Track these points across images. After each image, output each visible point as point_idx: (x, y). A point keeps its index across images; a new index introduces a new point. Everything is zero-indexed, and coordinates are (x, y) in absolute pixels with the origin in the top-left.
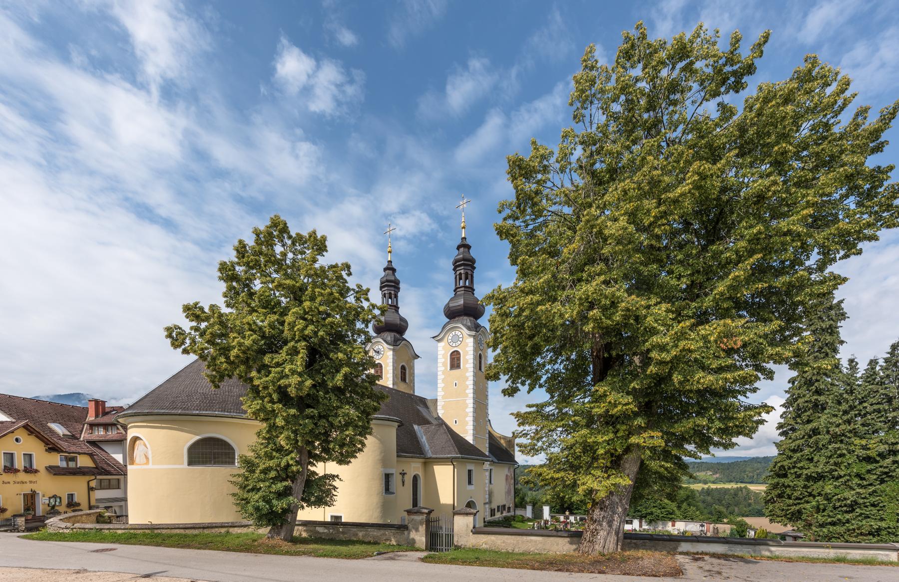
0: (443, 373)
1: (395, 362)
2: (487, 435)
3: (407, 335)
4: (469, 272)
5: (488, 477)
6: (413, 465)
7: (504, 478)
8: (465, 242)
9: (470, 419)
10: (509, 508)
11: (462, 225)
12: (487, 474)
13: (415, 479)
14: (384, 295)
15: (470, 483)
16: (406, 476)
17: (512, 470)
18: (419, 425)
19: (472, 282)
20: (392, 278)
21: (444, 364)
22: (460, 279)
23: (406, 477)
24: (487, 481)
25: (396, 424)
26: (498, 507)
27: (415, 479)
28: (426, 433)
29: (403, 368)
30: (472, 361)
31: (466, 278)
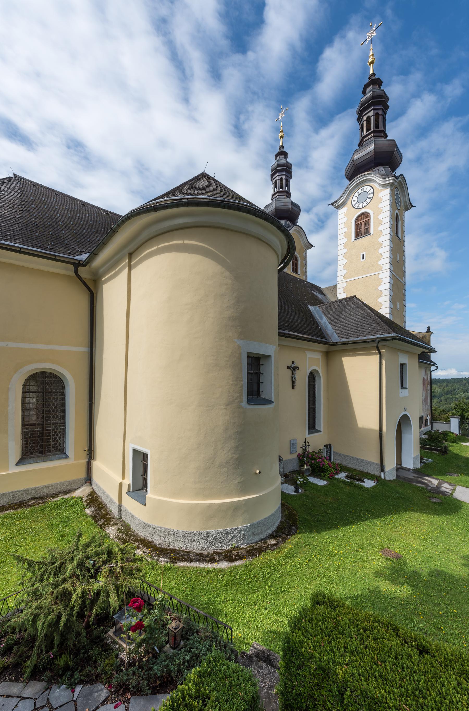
0: (345, 245)
4: (381, 112)
6: (310, 355)
10: (426, 420)
11: (370, 60)
13: (312, 377)
16: (297, 372)
17: (428, 373)
20: (284, 161)
21: (347, 235)
23: (298, 374)
27: (312, 377)
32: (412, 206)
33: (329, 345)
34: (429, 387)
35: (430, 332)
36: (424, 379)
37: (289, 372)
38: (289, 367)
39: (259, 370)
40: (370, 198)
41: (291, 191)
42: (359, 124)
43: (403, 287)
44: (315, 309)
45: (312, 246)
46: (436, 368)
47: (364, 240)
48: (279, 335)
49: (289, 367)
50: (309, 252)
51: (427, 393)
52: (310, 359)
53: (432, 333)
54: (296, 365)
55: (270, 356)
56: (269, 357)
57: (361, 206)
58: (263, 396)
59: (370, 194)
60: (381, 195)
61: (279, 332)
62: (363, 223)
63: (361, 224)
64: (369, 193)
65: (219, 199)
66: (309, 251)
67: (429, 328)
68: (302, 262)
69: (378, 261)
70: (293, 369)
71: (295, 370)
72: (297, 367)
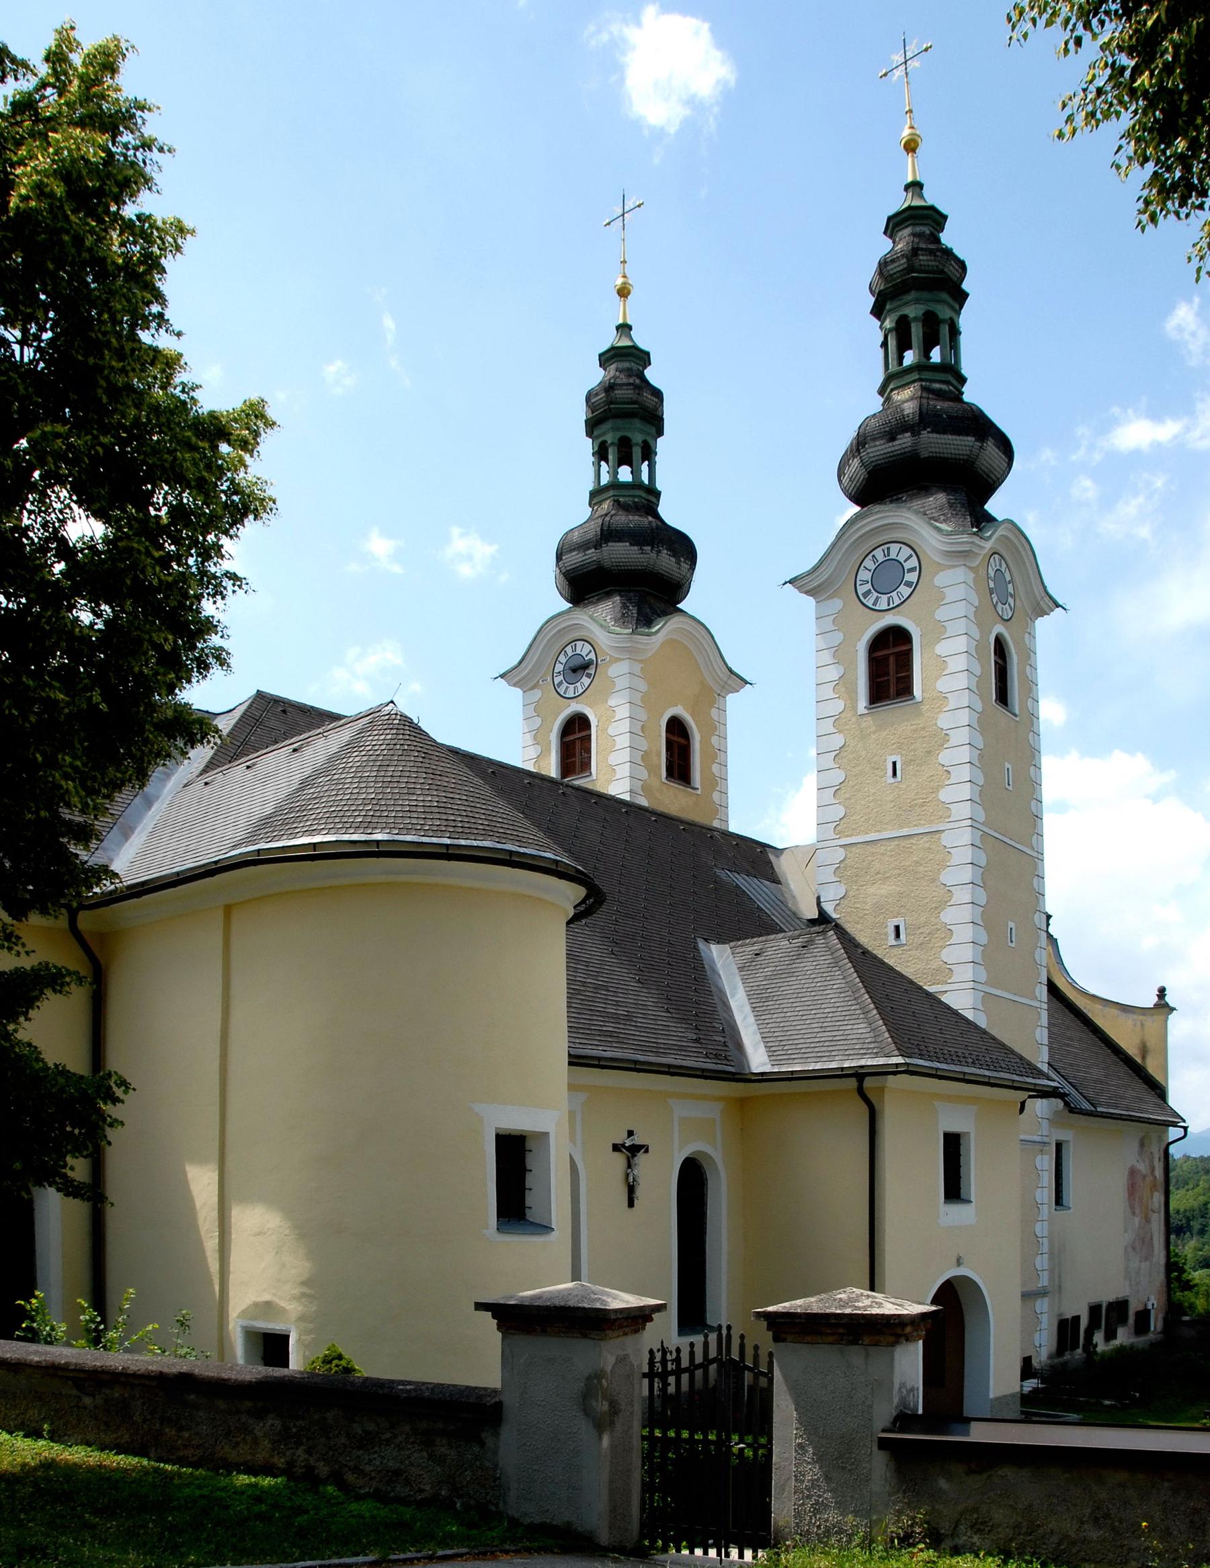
5: (1048, 1179)
9: (960, 916)
12: (1046, 1162)
13: (693, 1179)
14: (601, 454)
15: (954, 1191)
16: (641, 1158)
18: (720, 941)
24: (1046, 1194)
25: (571, 893)
26: (1095, 1310)
34: (1158, 1197)
35: (1167, 1005)
36: (1133, 1172)
37: (620, 1160)
38: (616, 1148)
40: (908, 584)
43: (1035, 867)
46: (1181, 1132)
48: (570, 1064)
49: (616, 1148)
51: (1148, 1220)
53: (1173, 1009)
54: (637, 1140)
55: (547, 1134)
59: (910, 570)
60: (941, 579)
61: (570, 1055)
62: (892, 659)
63: (886, 658)
64: (907, 566)
65: (435, 840)
66: (731, 698)
67: (1162, 992)
68: (706, 742)
69: (936, 790)
71: (634, 1156)
72: (643, 1146)
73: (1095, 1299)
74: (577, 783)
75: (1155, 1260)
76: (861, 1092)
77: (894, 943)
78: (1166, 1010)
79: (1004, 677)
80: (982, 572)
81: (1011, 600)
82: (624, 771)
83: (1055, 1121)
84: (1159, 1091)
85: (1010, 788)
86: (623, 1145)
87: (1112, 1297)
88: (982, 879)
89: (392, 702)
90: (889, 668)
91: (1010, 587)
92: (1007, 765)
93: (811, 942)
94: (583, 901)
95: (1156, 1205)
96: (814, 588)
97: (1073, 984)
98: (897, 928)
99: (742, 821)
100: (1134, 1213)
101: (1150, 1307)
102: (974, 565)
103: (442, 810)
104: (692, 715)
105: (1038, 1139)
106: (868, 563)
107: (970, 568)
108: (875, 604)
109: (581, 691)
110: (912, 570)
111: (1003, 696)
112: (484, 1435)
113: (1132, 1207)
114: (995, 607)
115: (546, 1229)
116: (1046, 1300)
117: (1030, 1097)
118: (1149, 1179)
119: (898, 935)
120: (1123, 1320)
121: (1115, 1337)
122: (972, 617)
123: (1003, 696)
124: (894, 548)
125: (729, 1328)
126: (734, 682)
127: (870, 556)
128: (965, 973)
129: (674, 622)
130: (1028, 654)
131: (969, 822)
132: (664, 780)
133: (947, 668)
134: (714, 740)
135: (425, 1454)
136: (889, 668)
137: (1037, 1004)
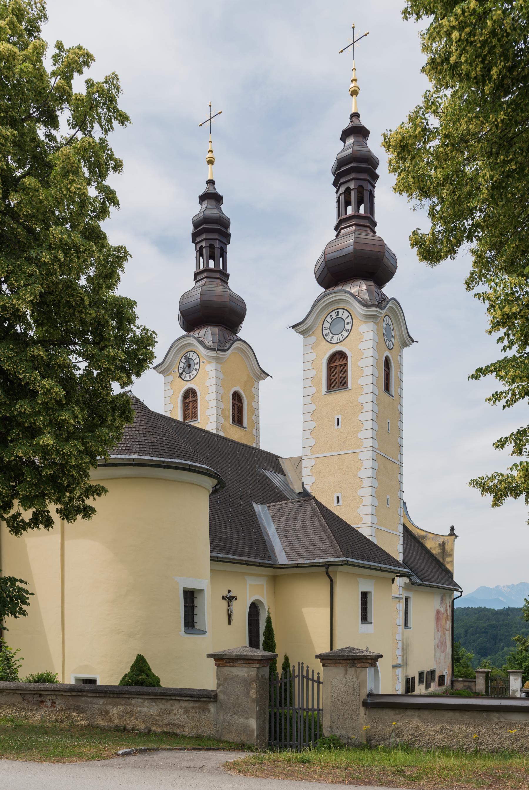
1: (221, 384)
2: (402, 526)
3: (245, 332)
5: (402, 614)
7: (432, 616)
8: (356, 123)
9: (365, 493)
12: (401, 606)
14: (200, 252)
15: (365, 618)
16: (234, 602)
17: (448, 602)
18: (263, 503)
19: (371, 209)
22: (348, 203)
26: (421, 674)
28: (276, 518)
29: (237, 397)
30: (369, 371)
31: (360, 202)
32: (413, 341)
33: (274, 568)
35: (454, 534)
36: (438, 612)
37: (225, 603)
38: (224, 598)
39: (193, 602)
41: (229, 271)
42: (337, 192)
44: (263, 509)
45: (268, 375)
46: (459, 594)
47: (339, 396)
48: (211, 560)
49: (224, 598)
50: (263, 384)
51: (444, 634)
52: (251, 589)
53: (457, 537)
54: (233, 594)
56: (202, 591)
57: (335, 340)
58: (197, 627)
61: (211, 557)
66: (261, 382)
67: (452, 528)
68: (249, 404)
70: (229, 599)
71: (231, 601)
72: (234, 597)
73: (421, 670)
74: (191, 423)
75: (447, 652)
76: (327, 573)
77: (336, 504)
78: (454, 537)
79: (388, 375)
80: (380, 325)
81: (393, 339)
82: (213, 418)
83: (406, 588)
84: (449, 575)
85: (389, 432)
86: (226, 596)
87: (428, 669)
88: (376, 475)
89: (130, 391)
90: (337, 371)
91: (392, 332)
92: (388, 421)
93: (303, 505)
94: (217, 485)
95: (448, 627)
96: (303, 331)
97: (413, 524)
98: (338, 498)
99: (266, 444)
100: (438, 631)
101: (444, 674)
102: (377, 322)
103: (159, 445)
104: (244, 391)
105: (398, 596)
106: (329, 319)
107: (375, 323)
108: (331, 340)
109: (192, 377)
110: (349, 323)
111: (387, 388)
112: (210, 707)
113: (437, 628)
114: (386, 343)
115: (203, 632)
116: (401, 669)
117: (397, 576)
118: (445, 615)
119: (338, 501)
120: (433, 679)
121: (430, 687)
122: (375, 348)
123: (387, 388)
124: (341, 312)
125: (303, 663)
126: (263, 375)
127: (329, 316)
128: (368, 519)
129: (236, 344)
130: (400, 365)
131: (371, 448)
132: (231, 423)
133: (363, 371)
134: (254, 404)
135: (185, 716)
136: (337, 371)
137: (398, 534)
